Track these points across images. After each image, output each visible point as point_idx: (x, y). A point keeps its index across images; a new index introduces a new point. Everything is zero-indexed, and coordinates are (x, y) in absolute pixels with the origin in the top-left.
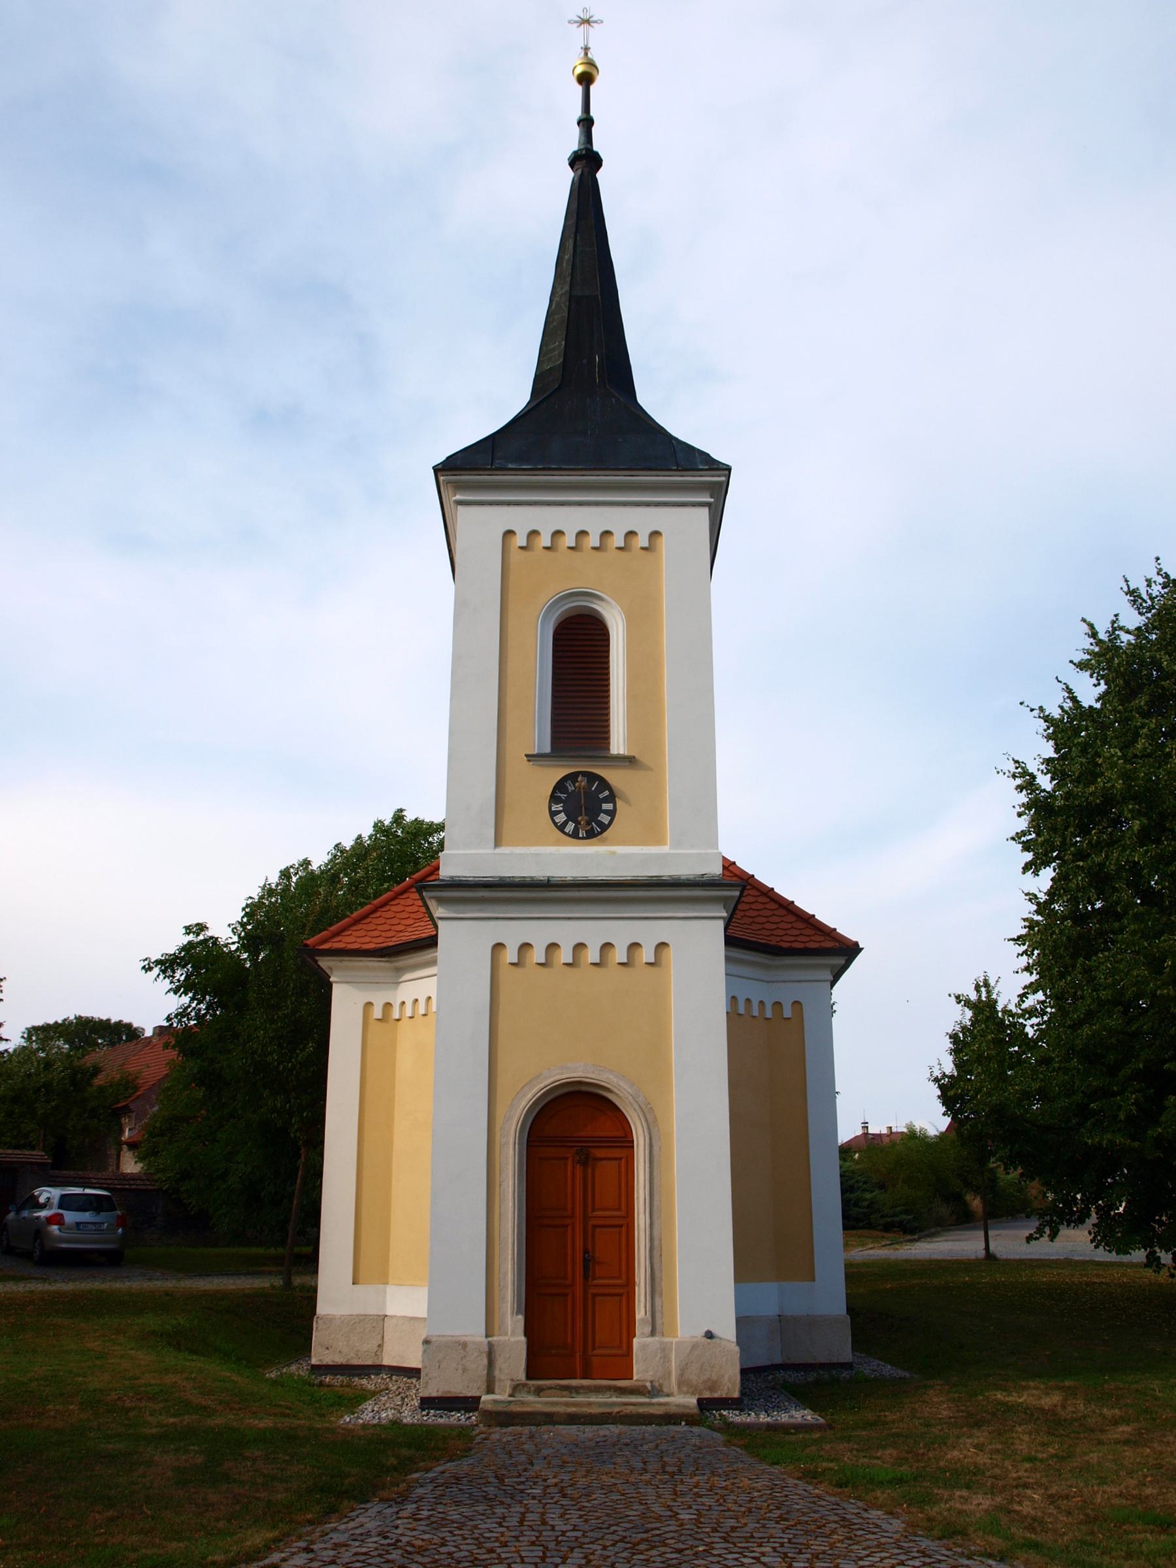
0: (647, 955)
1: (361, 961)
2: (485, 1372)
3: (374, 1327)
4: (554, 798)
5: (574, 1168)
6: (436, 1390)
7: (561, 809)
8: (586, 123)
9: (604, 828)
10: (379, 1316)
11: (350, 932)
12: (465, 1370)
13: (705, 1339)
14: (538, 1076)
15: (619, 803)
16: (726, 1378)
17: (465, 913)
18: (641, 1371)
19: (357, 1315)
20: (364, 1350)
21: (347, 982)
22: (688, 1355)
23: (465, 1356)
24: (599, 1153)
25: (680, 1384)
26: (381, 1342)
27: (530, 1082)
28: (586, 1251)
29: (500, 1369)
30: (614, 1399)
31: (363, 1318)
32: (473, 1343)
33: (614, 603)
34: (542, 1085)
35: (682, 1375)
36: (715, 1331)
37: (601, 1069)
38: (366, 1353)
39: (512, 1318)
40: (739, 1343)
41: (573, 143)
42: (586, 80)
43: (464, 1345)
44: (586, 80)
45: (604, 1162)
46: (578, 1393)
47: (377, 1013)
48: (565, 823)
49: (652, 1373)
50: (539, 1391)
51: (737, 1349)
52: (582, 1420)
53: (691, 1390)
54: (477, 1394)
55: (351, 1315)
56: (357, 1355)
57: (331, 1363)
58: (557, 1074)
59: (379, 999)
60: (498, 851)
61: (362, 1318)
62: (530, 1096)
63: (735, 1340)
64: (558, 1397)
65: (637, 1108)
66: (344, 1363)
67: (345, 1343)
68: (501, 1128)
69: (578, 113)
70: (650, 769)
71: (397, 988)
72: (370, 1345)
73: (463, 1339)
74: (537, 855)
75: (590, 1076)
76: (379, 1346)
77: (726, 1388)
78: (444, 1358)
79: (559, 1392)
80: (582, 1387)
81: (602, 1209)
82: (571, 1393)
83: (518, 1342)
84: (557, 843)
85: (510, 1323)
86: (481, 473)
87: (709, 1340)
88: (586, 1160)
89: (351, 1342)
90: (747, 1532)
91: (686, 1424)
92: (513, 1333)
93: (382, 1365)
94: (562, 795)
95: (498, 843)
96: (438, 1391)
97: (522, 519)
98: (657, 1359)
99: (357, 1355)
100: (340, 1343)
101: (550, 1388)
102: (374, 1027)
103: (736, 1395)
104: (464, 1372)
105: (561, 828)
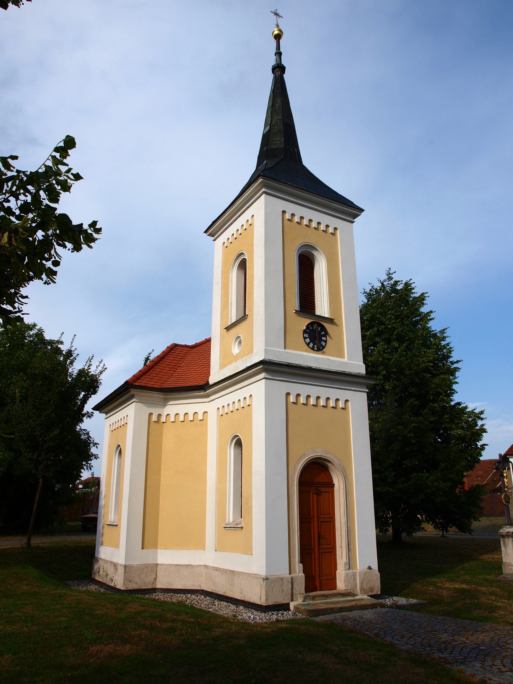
0: (341, 404)
1: (151, 393)
2: (291, 591)
3: (152, 570)
4: (305, 332)
5: (313, 497)
6: (271, 601)
7: (308, 336)
8: (279, 54)
9: (324, 347)
10: (155, 564)
11: (143, 379)
12: (282, 591)
13: (368, 570)
14: (305, 454)
15: (328, 338)
16: (376, 586)
17: (276, 377)
18: (341, 585)
19: (144, 564)
20: (148, 581)
21: (141, 402)
22: (363, 577)
23: (282, 584)
24: (323, 489)
25: (362, 589)
26: (156, 577)
27: (302, 456)
28: (319, 533)
29: (295, 589)
30: (341, 599)
31: (147, 566)
32: (286, 578)
33: (322, 253)
34: (307, 458)
35: (362, 586)
36: (372, 567)
37: (327, 452)
38: (149, 583)
39: (298, 564)
40: (379, 571)
41: (272, 61)
42: (278, 37)
43: (282, 579)
44: (278, 37)
45: (323, 493)
46: (328, 598)
47: (154, 418)
48: (309, 343)
49: (350, 586)
50: (314, 598)
51: (379, 573)
52: (344, 610)
53: (365, 592)
54: (288, 602)
55: (141, 564)
56: (144, 584)
57: (132, 589)
58: (311, 454)
59: (156, 412)
60: (286, 350)
61: (147, 565)
62: (302, 463)
63: (378, 570)
64: (321, 600)
65: (341, 470)
66: (138, 588)
67: (139, 578)
68: (291, 478)
69: (274, 51)
70: (337, 325)
71: (164, 408)
72: (151, 579)
73: (281, 576)
74: (302, 355)
75: (323, 455)
76: (155, 579)
77: (376, 590)
78: (274, 586)
79: (320, 598)
80: (330, 595)
81: (323, 514)
82: (325, 597)
83: (302, 576)
84: (306, 351)
85: (297, 567)
86: (278, 182)
87: (370, 570)
88: (318, 494)
89: (141, 578)
90: (454, 654)
91: (380, 608)
92: (299, 573)
93: (156, 588)
94: (308, 331)
95: (285, 348)
96: (272, 602)
97: (291, 208)
98: (352, 579)
99: (144, 584)
100: (136, 579)
101: (318, 596)
102: (153, 426)
103: (379, 593)
104: (282, 592)
105: (308, 344)
